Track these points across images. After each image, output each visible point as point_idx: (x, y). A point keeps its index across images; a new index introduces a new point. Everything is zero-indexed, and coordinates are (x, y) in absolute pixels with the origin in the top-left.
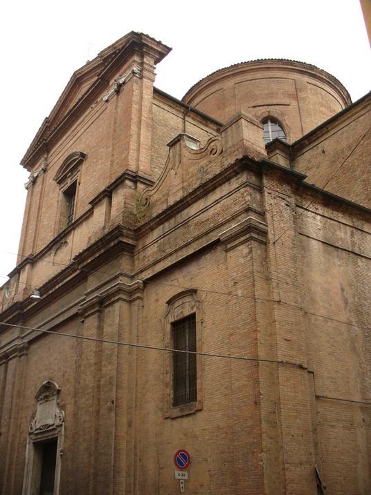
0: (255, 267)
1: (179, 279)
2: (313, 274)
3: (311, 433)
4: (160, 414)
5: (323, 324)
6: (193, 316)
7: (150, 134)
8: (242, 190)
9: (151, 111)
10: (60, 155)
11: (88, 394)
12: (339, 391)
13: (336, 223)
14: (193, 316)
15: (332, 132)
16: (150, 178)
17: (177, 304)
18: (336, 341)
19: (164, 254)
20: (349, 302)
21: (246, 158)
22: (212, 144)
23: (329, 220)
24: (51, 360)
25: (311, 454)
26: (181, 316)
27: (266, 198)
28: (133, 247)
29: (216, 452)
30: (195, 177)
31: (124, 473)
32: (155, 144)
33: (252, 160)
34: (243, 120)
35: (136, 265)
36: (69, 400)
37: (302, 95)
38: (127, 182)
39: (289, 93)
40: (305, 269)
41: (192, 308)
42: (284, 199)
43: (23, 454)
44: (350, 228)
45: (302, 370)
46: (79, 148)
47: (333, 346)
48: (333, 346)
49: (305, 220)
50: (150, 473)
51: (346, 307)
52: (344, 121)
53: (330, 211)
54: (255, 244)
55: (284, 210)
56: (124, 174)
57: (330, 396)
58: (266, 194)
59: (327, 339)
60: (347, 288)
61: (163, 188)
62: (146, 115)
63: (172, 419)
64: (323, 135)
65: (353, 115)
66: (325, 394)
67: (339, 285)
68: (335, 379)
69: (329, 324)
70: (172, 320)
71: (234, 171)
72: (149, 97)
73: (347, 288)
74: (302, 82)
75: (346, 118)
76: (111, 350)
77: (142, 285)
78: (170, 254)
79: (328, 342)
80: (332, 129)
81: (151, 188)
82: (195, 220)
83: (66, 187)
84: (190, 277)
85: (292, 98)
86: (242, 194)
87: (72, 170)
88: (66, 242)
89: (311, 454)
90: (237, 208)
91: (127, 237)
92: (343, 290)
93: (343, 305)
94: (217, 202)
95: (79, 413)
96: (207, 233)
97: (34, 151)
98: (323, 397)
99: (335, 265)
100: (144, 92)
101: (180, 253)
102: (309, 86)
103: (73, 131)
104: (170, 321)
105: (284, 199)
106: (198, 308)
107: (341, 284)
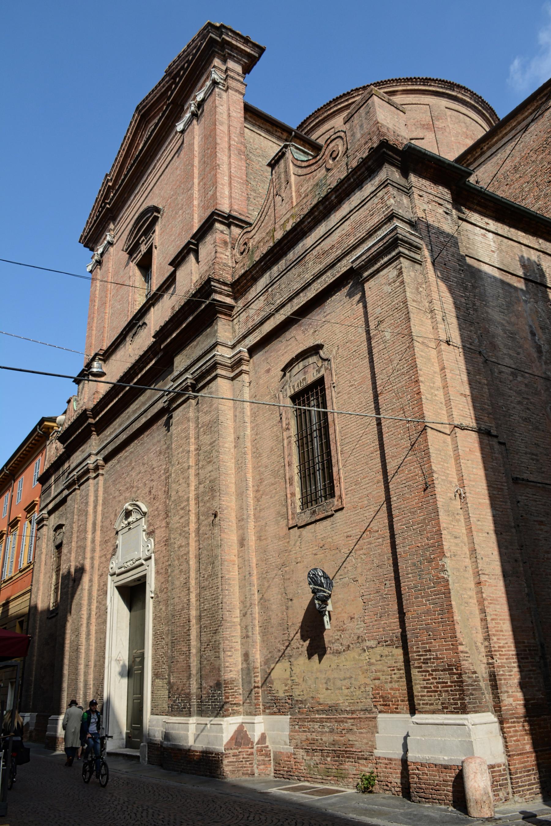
0: (408, 294)
1: (297, 337)
2: (490, 311)
3: (514, 530)
4: (283, 523)
5: (511, 378)
6: (320, 382)
7: (243, 164)
8: (380, 194)
9: (242, 134)
10: (128, 220)
11: (182, 509)
12: (543, 472)
13: (516, 244)
14: (320, 382)
15: (489, 153)
16: (247, 220)
17: (296, 370)
18: (531, 403)
19: (273, 307)
20: (544, 350)
21: (384, 144)
22: (331, 145)
23: (506, 240)
24: (134, 474)
25: (516, 561)
26: (304, 384)
27: (417, 202)
28: (231, 308)
29: (369, 567)
30: (310, 196)
31: (237, 612)
32: (251, 179)
33: (393, 148)
34: (375, 98)
35: (237, 331)
36: (158, 523)
37: (439, 124)
38: (217, 225)
39: (422, 123)
40: (478, 304)
41: (318, 371)
42: (441, 205)
43: (103, 603)
44: (535, 251)
45: (490, 438)
46: (150, 203)
47: (528, 409)
48: (528, 409)
49: (471, 238)
50: (274, 607)
51: (540, 357)
52: (506, 134)
53: (506, 228)
54: (405, 263)
55: (443, 220)
56: (213, 214)
57: (532, 479)
58: (416, 196)
59: (519, 399)
60: (539, 332)
61: (267, 223)
62: (236, 139)
63: (300, 528)
64: (475, 160)
65: (519, 123)
66: (525, 476)
67: (527, 327)
68: (536, 455)
69: (519, 379)
70: (290, 392)
71: (366, 169)
72: (239, 115)
73: (539, 332)
74: (439, 107)
75: (508, 129)
76: (211, 444)
77: (247, 355)
78: (283, 306)
79: (519, 403)
80: (489, 148)
81: (249, 229)
82: (315, 252)
83: (139, 257)
84: (312, 331)
85: (427, 128)
86: (382, 198)
87: (146, 233)
88: (145, 324)
89: (516, 561)
90: (376, 219)
91: (220, 293)
92: (533, 334)
93: (535, 355)
94: (345, 219)
95: (172, 536)
96: (332, 266)
97: (98, 217)
98: (523, 480)
99: (519, 301)
100: (231, 109)
101: (295, 301)
102: (449, 112)
103: (143, 184)
104: (289, 394)
105: (441, 205)
106: (326, 369)
107: (530, 326)
